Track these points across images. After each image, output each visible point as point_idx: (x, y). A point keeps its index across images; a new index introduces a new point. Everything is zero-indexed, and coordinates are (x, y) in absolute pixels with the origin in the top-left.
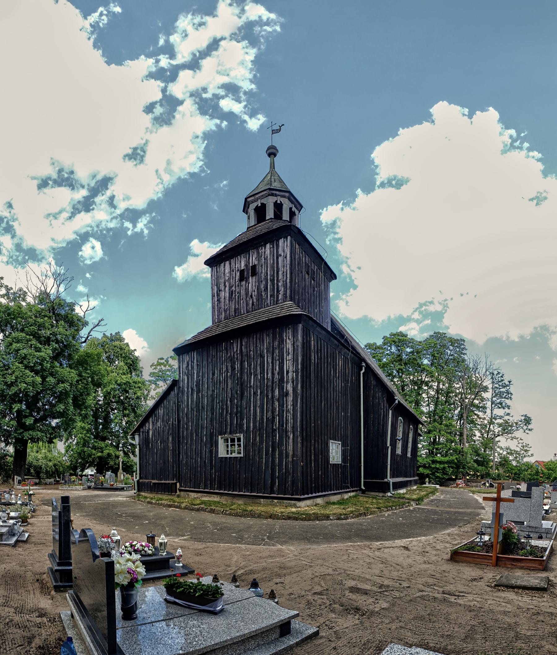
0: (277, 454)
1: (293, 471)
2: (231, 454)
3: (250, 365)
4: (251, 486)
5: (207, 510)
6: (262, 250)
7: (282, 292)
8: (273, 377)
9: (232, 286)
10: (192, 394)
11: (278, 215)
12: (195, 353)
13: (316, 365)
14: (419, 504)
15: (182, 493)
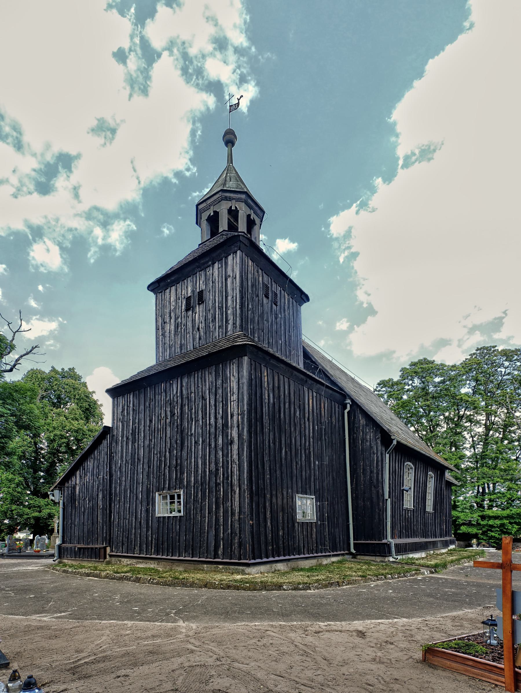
1: (240, 531)
2: (171, 513)
4: (192, 550)
5: (132, 579)
6: (209, 272)
7: (231, 322)
9: (178, 317)
10: (127, 443)
11: (232, 227)
12: (131, 396)
13: (271, 406)
14: (436, 572)
15: (113, 559)
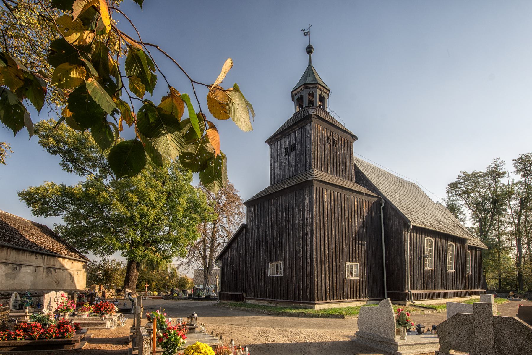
0: (302, 273)
3: (286, 215)
8: (299, 222)
9: (281, 159)
